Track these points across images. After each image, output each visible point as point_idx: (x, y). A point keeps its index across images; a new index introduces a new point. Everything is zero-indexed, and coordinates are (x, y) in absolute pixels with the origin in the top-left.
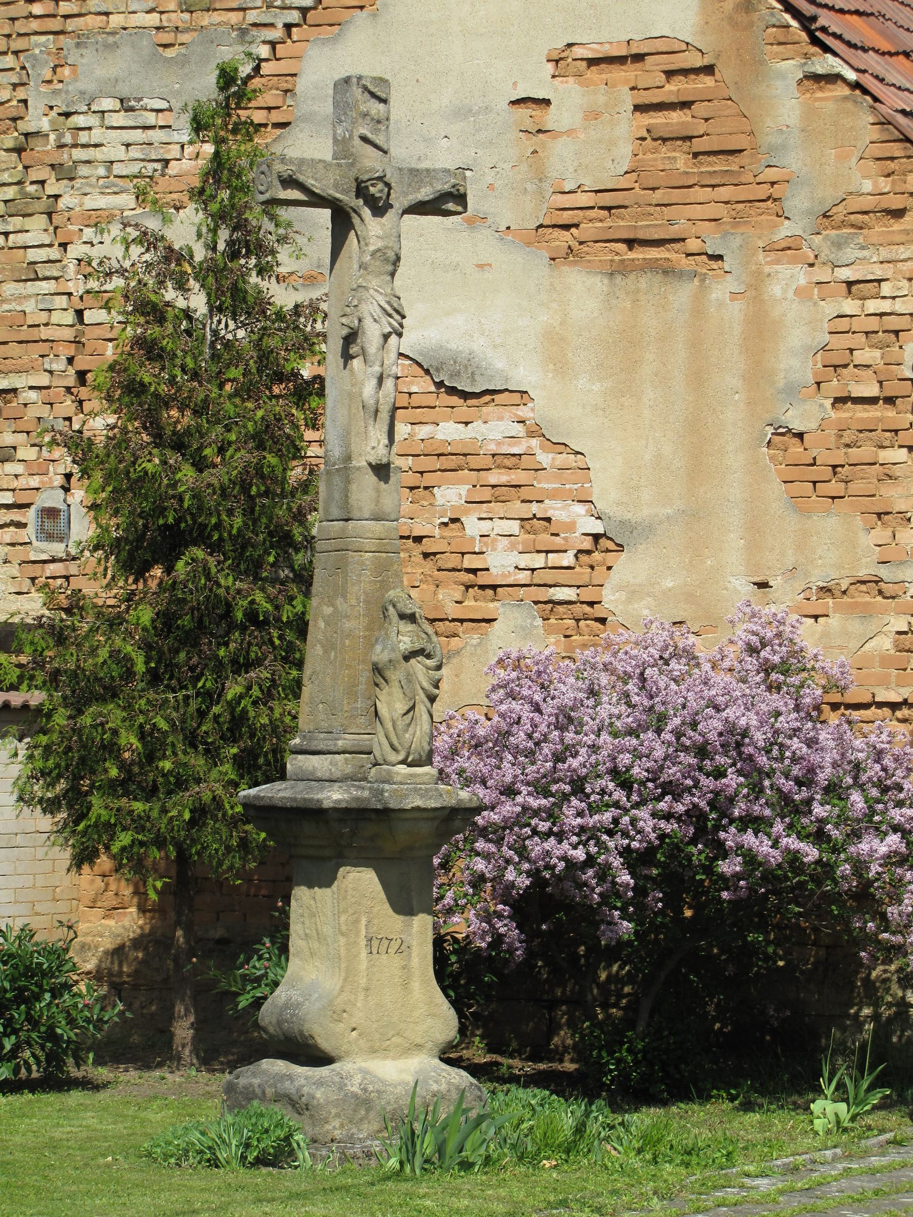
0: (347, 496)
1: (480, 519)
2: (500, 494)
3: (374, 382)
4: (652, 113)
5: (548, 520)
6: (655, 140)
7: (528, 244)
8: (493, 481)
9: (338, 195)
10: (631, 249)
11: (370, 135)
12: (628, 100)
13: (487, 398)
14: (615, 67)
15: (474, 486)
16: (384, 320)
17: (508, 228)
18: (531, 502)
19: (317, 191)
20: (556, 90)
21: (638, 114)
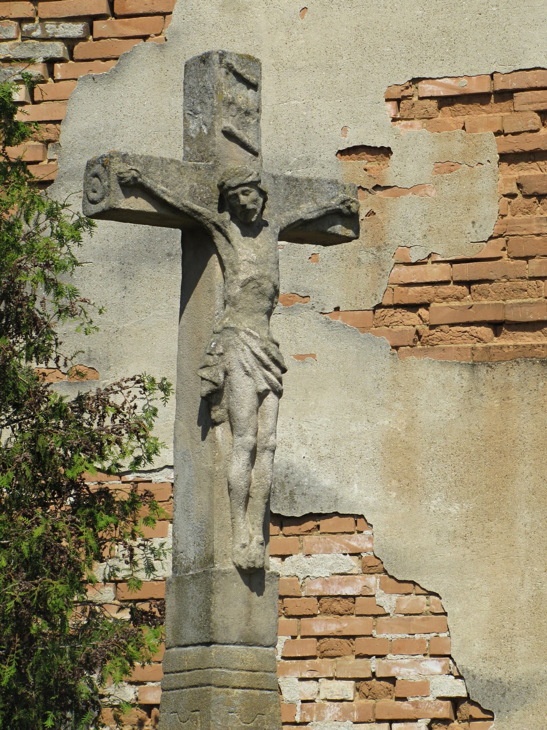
0: (208, 611)
1: (302, 679)
2: (327, 647)
3: (245, 457)
4: (523, 164)
5: (392, 680)
6: (527, 196)
7: (364, 329)
8: (318, 630)
9: (196, 207)
10: (497, 335)
11: (235, 130)
12: (493, 147)
13: (311, 524)
14: (474, 107)
15: (294, 637)
16: (260, 373)
17: (337, 309)
18: (369, 657)
19: (169, 200)
20: (398, 136)
21: (504, 165)
